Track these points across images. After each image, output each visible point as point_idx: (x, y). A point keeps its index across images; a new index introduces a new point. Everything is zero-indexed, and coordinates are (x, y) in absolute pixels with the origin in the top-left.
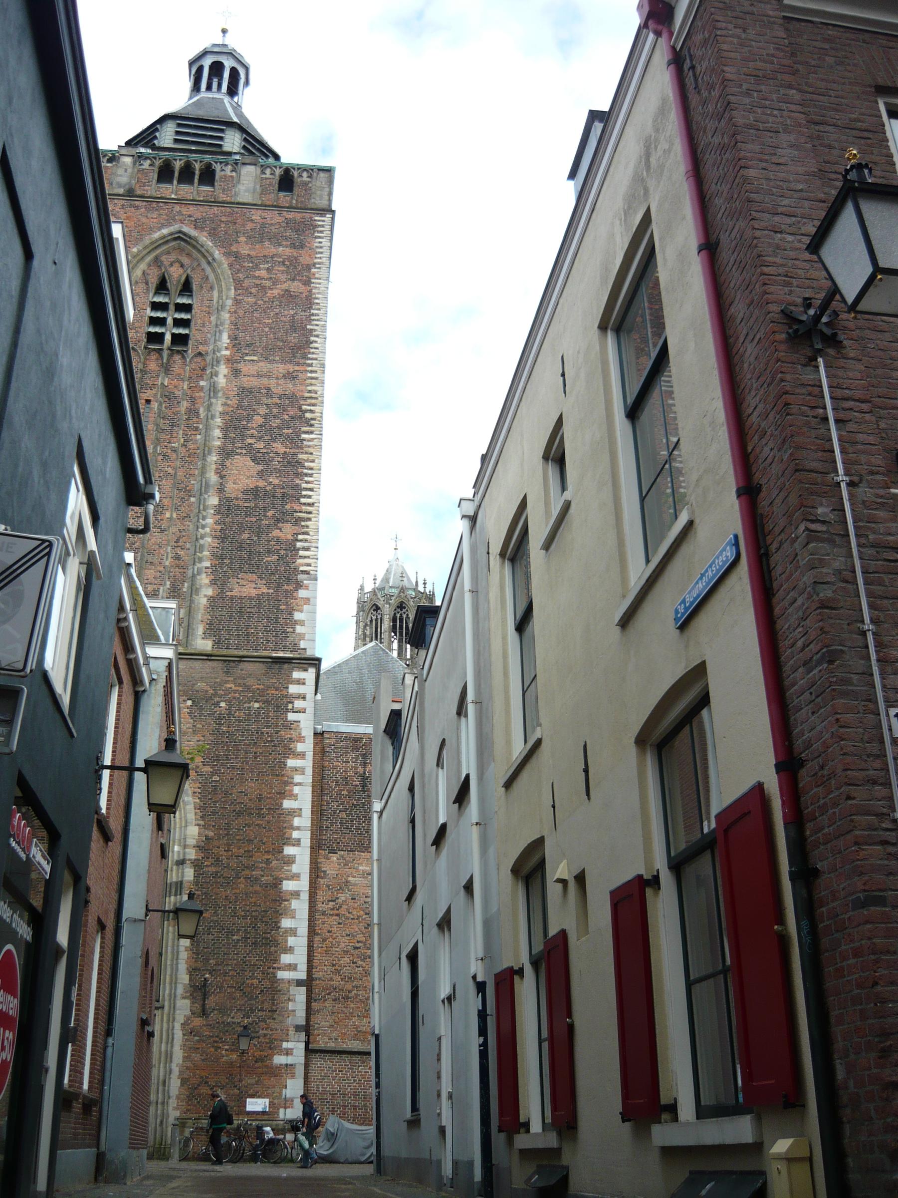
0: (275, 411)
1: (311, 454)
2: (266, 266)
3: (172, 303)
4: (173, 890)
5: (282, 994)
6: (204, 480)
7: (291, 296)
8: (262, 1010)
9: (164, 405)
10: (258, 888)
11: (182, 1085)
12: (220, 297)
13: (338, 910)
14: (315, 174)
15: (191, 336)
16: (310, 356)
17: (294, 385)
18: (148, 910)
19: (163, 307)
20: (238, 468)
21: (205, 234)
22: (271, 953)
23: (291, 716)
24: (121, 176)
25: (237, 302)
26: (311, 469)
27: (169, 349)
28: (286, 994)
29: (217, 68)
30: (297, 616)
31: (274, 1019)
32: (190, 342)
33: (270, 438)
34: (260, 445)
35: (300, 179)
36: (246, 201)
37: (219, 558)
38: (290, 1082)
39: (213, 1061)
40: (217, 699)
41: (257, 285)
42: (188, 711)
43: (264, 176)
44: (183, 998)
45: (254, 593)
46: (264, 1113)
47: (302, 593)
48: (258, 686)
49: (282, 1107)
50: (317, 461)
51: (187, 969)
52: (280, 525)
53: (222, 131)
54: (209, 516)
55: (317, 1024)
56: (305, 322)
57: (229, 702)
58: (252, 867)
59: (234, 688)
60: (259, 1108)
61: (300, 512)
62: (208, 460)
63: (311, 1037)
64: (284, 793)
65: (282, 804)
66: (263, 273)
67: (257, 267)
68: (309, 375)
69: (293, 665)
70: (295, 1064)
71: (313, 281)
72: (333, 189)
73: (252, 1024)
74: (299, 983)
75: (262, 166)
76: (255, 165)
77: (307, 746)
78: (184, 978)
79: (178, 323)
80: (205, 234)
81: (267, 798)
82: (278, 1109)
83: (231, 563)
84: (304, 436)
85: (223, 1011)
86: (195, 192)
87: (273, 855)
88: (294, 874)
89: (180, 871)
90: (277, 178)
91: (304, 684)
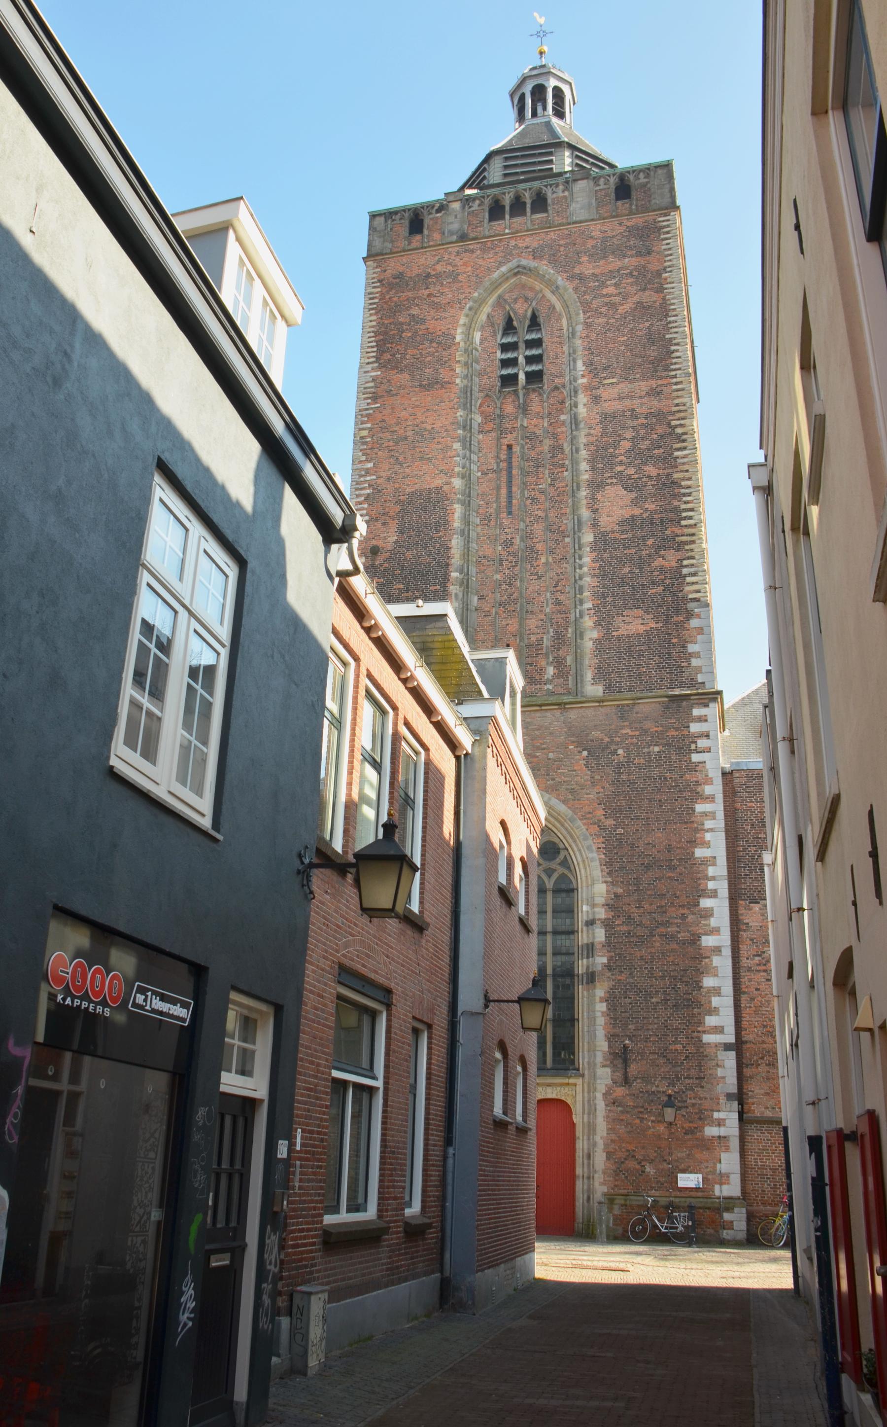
0: (642, 432)
1: (687, 471)
2: (613, 281)
3: (521, 340)
4: (585, 953)
5: (709, 1060)
6: (576, 517)
7: (644, 307)
8: (688, 1077)
9: (526, 447)
10: (675, 946)
11: (608, 1158)
12: (570, 324)
13: (765, 965)
14: (652, 173)
15: (545, 371)
16: (673, 367)
17: (659, 401)
18: (487, 1001)
19: (513, 347)
20: (610, 500)
21: (545, 262)
22: (693, 1015)
23: (695, 758)
24: (452, 223)
25: (588, 325)
26: (689, 487)
27: (524, 388)
28: (714, 1060)
29: (539, 92)
30: (692, 648)
31: (702, 1087)
32: (545, 377)
33: (640, 462)
34: (631, 471)
35: (637, 182)
36: (582, 218)
37: (600, 596)
38: (724, 1156)
39: (638, 1133)
40: (613, 747)
41: (606, 304)
42: (584, 762)
43: (598, 188)
44: (604, 1066)
45: (641, 629)
46: (697, 1189)
47: (694, 623)
48: (656, 729)
49: (716, 1183)
50: (693, 478)
51: (606, 1035)
52: (662, 553)
53: (551, 154)
54: (585, 554)
55: (751, 1091)
56: (663, 332)
57: (627, 750)
58: (667, 924)
59: (630, 733)
60: (692, 1185)
61: (682, 535)
62: (578, 496)
63: (746, 1107)
64: (695, 841)
65: (693, 853)
66: (611, 290)
67: (603, 285)
68: (675, 387)
69: (692, 701)
70: (729, 1136)
71: (666, 286)
72: (673, 183)
73: (679, 1092)
74: (727, 1047)
75: (594, 178)
76: (587, 178)
77: (715, 789)
78: (603, 1045)
79: (530, 360)
80: (545, 262)
81: (677, 848)
82: (713, 1186)
83: (614, 601)
84: (676, 454)
85: (646, 1079)
86: (529, 222)
87: (689, 909)
88: (713, 928)
89: (590, 932)
90: (613, 187)
91: (706, 721)
